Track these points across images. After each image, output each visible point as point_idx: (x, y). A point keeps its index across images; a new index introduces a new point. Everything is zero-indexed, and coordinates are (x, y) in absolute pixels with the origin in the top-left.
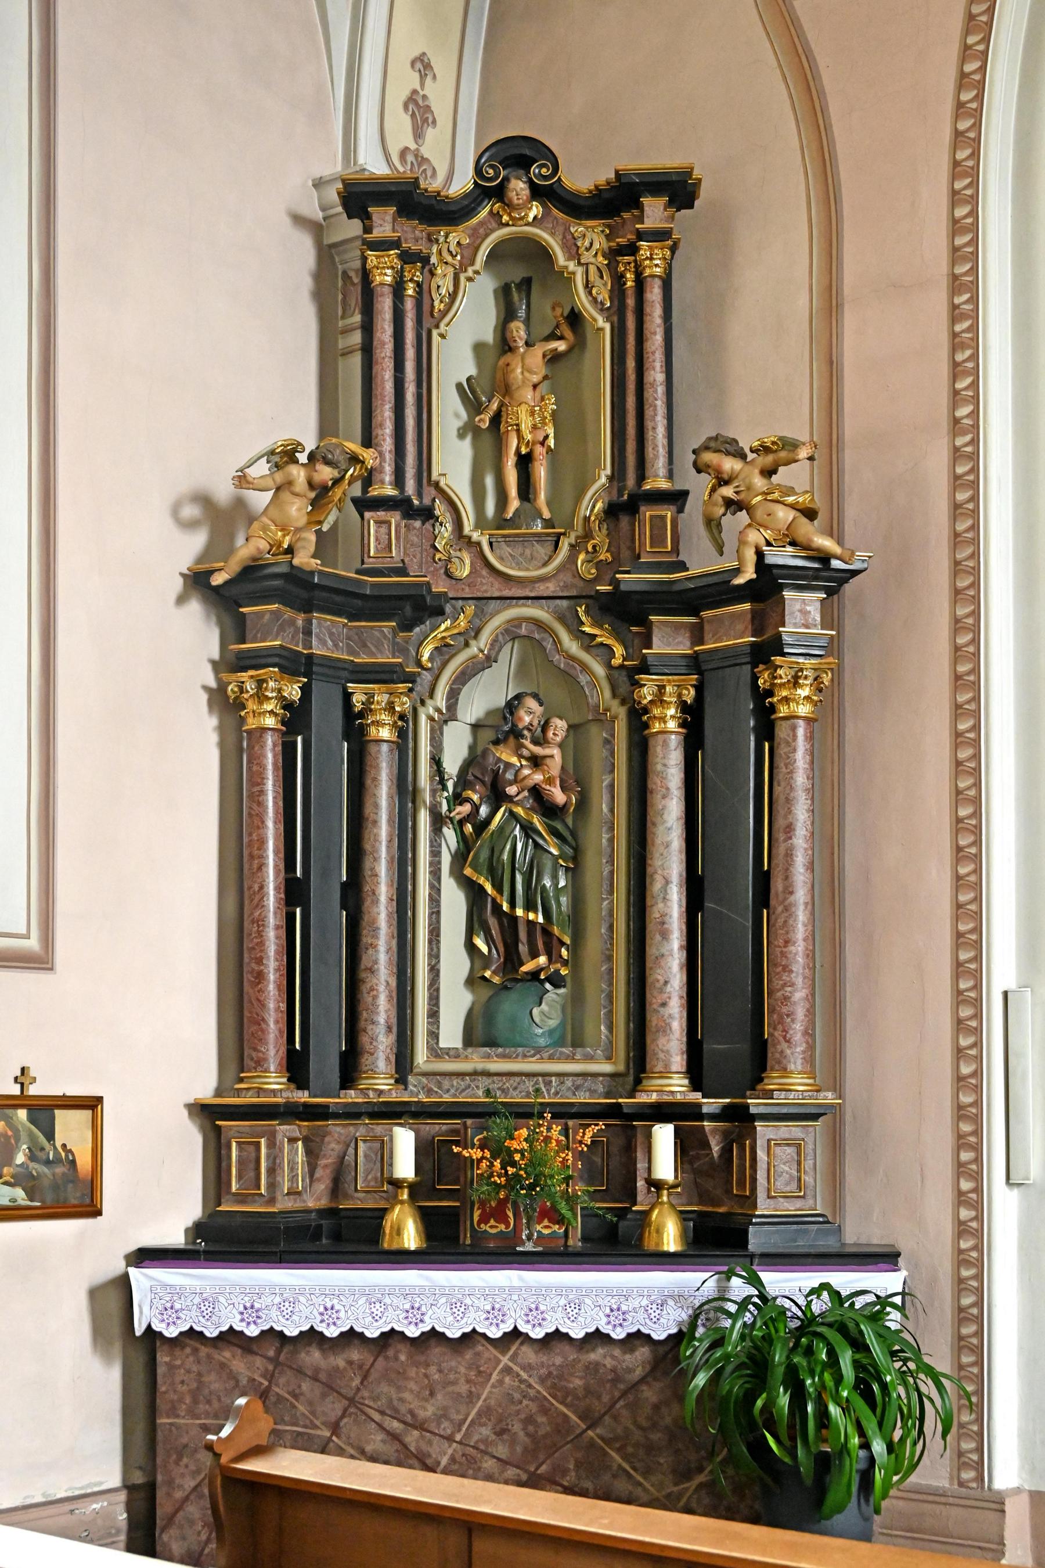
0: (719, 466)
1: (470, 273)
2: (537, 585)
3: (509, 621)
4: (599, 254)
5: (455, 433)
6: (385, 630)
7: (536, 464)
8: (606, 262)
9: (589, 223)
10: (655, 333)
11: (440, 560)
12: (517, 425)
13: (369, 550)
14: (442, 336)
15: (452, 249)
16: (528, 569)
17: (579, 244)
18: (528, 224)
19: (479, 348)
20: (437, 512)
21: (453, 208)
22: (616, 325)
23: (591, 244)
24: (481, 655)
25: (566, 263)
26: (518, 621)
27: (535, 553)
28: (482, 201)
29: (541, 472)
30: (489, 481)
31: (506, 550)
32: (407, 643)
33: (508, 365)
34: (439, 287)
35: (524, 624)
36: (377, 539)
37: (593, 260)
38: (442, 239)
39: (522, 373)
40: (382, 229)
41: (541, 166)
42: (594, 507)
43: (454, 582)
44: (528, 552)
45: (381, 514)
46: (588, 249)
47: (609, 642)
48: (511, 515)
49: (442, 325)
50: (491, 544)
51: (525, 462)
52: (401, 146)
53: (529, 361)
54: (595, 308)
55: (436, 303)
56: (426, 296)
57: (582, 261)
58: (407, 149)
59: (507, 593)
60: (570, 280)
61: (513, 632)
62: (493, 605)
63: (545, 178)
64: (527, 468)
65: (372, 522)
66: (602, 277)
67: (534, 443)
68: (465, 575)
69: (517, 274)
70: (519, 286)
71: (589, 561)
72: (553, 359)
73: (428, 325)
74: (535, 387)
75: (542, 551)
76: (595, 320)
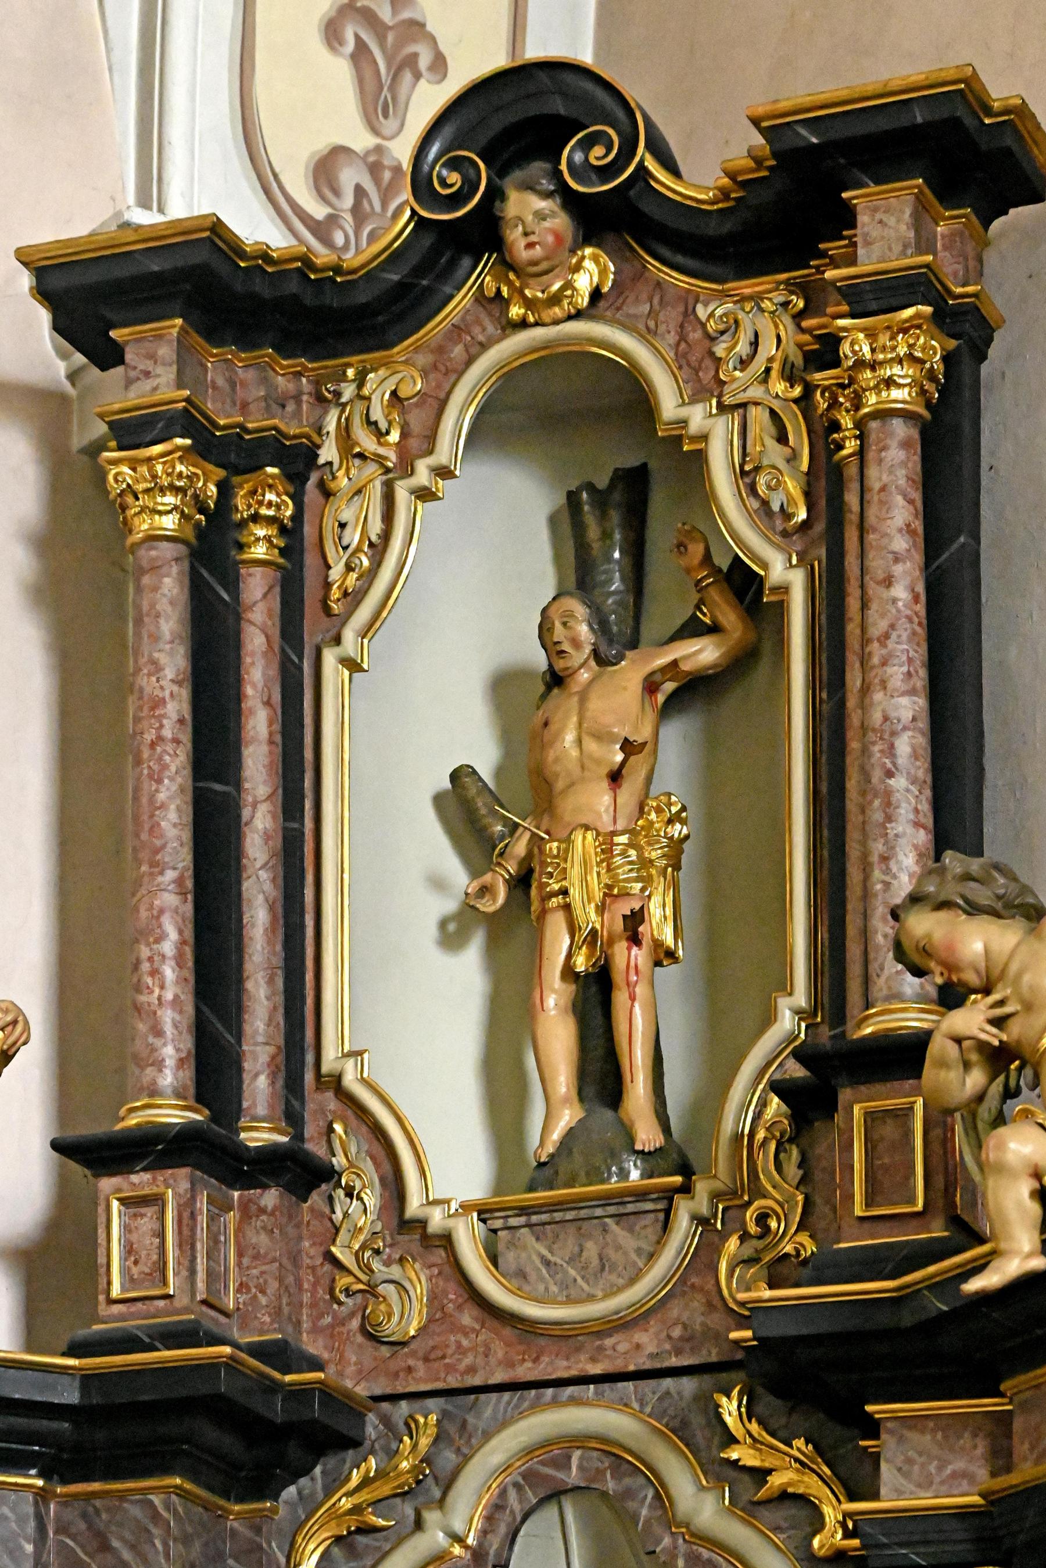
0: (950, 948)
1: (422, 476)
2: (608, 1342)
3: (529, 1451)
4: (774, 374)
5: (432, 931)
6: (156, 1499)
9: (747, 287)
10: (888, 582)
13: (109, 1283)
14: (353, 665)
15: (377, 414)
17: (720, 350)
18: (578, 315)
21: (362, 297)
23: (755, 344)
24: (457, 1550)
25: (683, 412)
26: (558, 1448)
27: (611, 1252)
28: (453, 263)
31: (531, 1249)
32: (258, 1530)
33: (546, 724)
34: (343, 526)
35: (576, 1455)
36: (129, 1250)
37: (755, 392)
38: (348, 391)
39: (579, 741)
40: (147, 385)
41: (587, 144)
43: (385, 1351)
44: (591, 1249)
45: (141, 1181)
46: (744, 363)
47: (812, 1485)
49: (349, 635)
51: (595, 993)
52: (321, 144)
53: (595, 704)
55: (335, 573)
56: (311, 560)
58: (338, 153)
59: (525, 1372)
61: (547, 1478)
62: (491, 1405)
63: (606, 172)
65: (115, 1205)
66: (782, 438)
67: (611, 942)
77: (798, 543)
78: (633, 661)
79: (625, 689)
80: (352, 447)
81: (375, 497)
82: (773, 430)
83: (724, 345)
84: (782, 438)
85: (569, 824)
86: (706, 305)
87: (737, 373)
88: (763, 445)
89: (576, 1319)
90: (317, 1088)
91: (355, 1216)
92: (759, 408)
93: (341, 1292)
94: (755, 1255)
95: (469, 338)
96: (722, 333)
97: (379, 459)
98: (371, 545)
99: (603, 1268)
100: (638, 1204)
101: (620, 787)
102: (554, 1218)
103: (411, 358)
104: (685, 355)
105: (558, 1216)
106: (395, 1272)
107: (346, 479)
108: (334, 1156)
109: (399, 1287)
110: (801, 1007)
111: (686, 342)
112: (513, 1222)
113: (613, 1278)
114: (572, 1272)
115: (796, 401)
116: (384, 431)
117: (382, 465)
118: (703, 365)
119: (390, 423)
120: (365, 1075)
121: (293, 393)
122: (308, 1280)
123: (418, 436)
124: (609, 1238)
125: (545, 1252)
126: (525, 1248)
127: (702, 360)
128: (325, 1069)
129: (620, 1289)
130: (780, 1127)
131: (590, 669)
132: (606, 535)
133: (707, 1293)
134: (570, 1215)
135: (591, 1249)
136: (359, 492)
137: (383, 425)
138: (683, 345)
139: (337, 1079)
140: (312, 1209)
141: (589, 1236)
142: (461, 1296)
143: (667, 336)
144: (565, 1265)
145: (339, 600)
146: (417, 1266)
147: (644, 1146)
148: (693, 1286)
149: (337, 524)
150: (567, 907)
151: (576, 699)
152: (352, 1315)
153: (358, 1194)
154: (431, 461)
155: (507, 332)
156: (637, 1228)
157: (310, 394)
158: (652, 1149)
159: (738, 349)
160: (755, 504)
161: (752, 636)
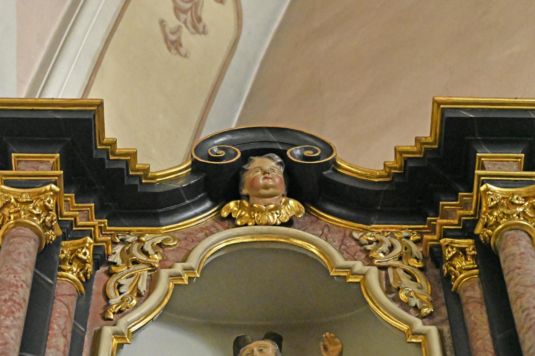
8: (420, 265)
66: (414, 279)
84: (414, 279)
104: (344, 250)
117: (152, 266)
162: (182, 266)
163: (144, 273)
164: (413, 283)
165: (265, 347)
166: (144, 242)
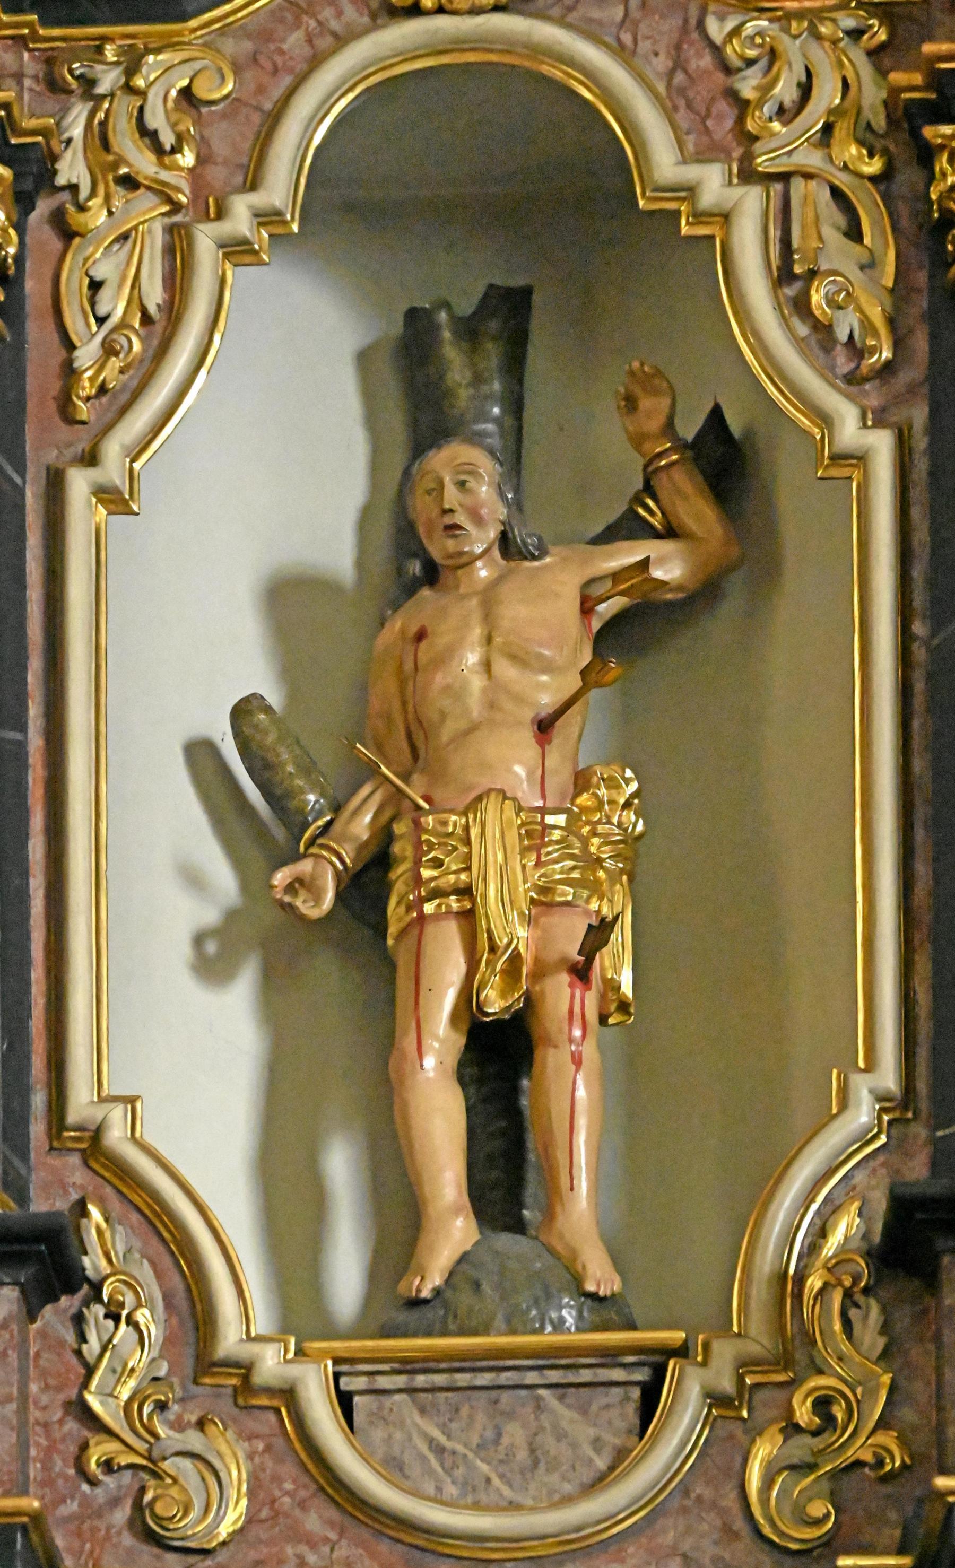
4: (841, 130)
7: (553, 1061)
8: (874, 167)
11: (108, 1466)
12: (465, 892)
14: (115, 500)
15: (156, 119)
16: (513, 1507)
17: (748, 87)
19: (289, 600)
20: (93, 1263)
22: (921, 443)
23: (806, 90)
25: (692, 172)
27: (548, 1441)
29: (574, 1095)
30: (341, 1165)
31: (416, 1427)
34: (96, 286)
37: (812, 159)
38: (108, 80)
39: (487, 666)
42: (821, 1232)
44: (515, 1434)
48: (435, 1279)
49: (113, 450)
50: (345, 1401)
51: (499, 1054)
53: (516, 611)
54: (827, 373)
57: (762, 163)
60: (706, 254)
64: (514, 1091)
66: (854, 233)
67: (540, 972)
68: (224, 1530)
69: (462, 281)
70: (469, 331)
71: (801, 1468)
72: (632, 630)
73: (51, 456)
74: (544, 727)
75: (586, 1426)
76: (825, 420)
77: (874, 396)
78: (564, 559)
79: (557, 595)
80: (115, 166)
81: (152, 247)
82: (841, 220)
83: (754, 82)
84: (854, 233)
85: (470, 788)
86: (722, 18)
87: (776, 126)
88: (821, 239)
89: (508, 1534)
90: (52, 1149)
91: (124, 1350)
92: (813, 184)
93: (98, 1465)
94: (809, 1459)
95: (313, 23)
96: (750, 63)
97: (164, 193)
98: (146, 319)
99: (536, 1463)
100: (600, 1371)
101: (550, 742)
102: (455, 1381)
103: (212, 42)
104: (682, 91)
105: (462, 1379)
106: (194, 1440)
107: (105, 212)
108: (86, 1253)
109: (201, 1466)
110: (889, 1091)
111: (686, 72)
112: (383, 1382)
113: (554, 1479)
114: (484, 1467)
115: (873, 179)
116: (168, 147)
117: (169, 200)
118: (714, 111)
119: (180, 138)
120: (138, 1135)
121: (14, 68)
122: (38, 1445)
123: (225, 163)
124: (545, 1420)
125: (436, 1433)
126: (402, 1424)
127: (713, 100)
128: (72, 1117)
129: (568, 1500)
130: (851, 1267)
131: (491, 564)
132: (478, 380)
133: (723, 1512)
134: (484, 1379)
135: (515, 1434)
136: (125, 237)
137: (168, 139)
138: (679, 78)
139: (97, 1134)
140: (43, 1334)
141: (510, 1415)
142: (305, 1487)
143: (655, 61)
144: (471, 1455)
145: (88, 399)
146: (230, 1434)
147: (598, 1285)
148: (699, 1499)
149: (86, 281)
150: (468, 917)
151: (474, 602)
152: (115, 1502)
153: (129, 1317)
154: (257, 199)
155: (379, 21)
156: (594, 1408)
157: (36, 78)
158: (609, 1293)
159: (777, 90)
160: (803, 330)
161: (735, 552)
162: (250, 207)
163: (147, 213)
164: (851, 244)
165: (470, 473)
166: (142, 94)
